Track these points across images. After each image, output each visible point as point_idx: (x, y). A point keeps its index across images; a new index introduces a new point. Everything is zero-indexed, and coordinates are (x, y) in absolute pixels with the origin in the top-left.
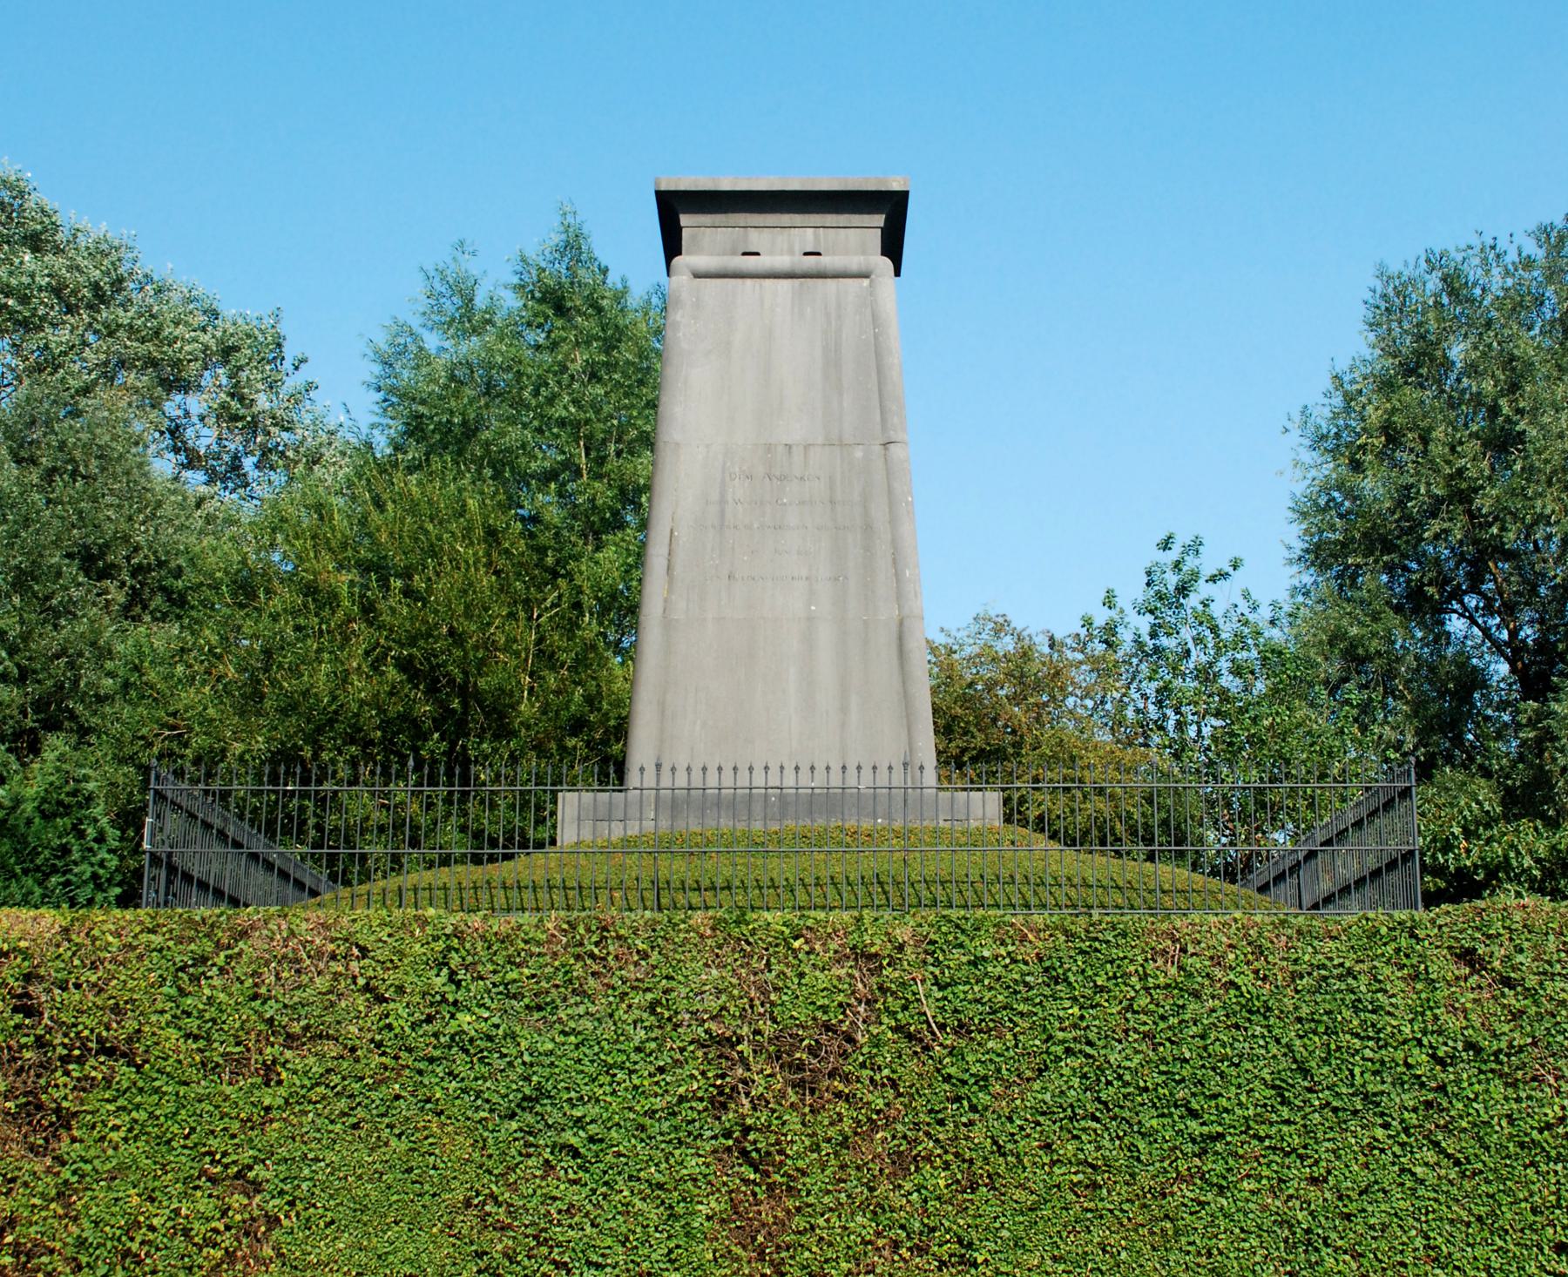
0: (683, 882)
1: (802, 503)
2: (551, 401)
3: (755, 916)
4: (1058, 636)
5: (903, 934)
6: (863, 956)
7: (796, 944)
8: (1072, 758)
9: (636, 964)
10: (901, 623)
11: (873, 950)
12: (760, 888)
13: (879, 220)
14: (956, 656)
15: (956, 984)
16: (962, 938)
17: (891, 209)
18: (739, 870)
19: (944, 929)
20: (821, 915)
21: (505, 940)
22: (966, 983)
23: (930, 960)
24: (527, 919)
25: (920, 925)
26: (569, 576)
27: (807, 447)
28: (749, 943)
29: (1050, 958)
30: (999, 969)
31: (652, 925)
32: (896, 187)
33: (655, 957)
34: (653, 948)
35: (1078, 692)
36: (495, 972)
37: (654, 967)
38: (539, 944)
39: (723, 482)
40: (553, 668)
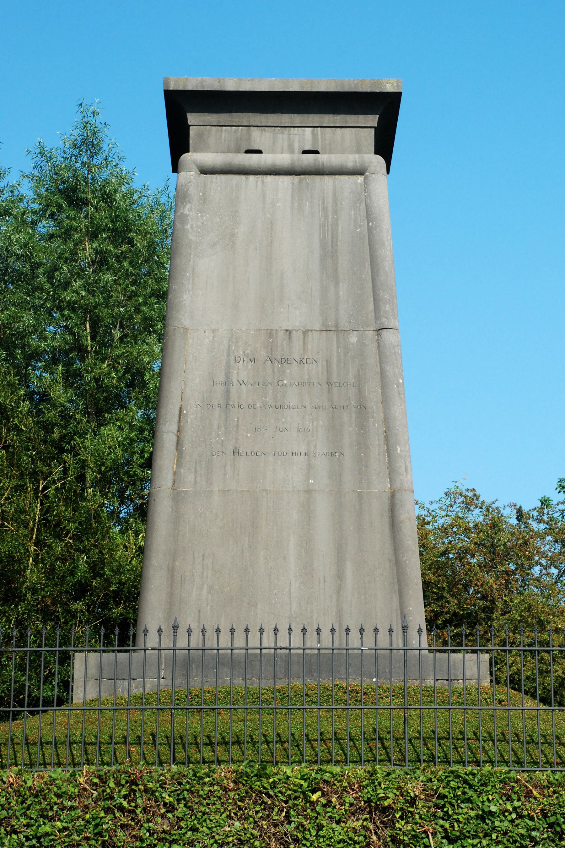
0: (125, 738)
1: (301, 384)
2: (66, 285)
3: (275, 770)
4: (526, 509)
5: (414, 788)
6: (378, 810)
7: (314, 797)
8: (541, 623)
9: (163, 816)
10: (393, 495)
11: (386, 803)
12: (268, 743)
13: (373, 120)
14: (429, 527)
15: (466, 837)
16: (470, 793)
17: (382, 110)
18: (270, 728)
19: (453, 784)
20: (337, 769)
21: (38, 794)
22: (475, 837)
23: (440, 814)
24: (58, 773)
25: (430, 780)
26: (74, 452)
27: (305, 333)
28: (269, 796)
29: (555, 814)
30: (506, 823)
31: (178, 779)
32: (389, 88)
33: (181, 809)
34: (179, 801)
35: (543, 562)
36: (28, 826)
37: (180, 819)
38: (71, 798)
39: (228, 363)
40: (59, 537)
